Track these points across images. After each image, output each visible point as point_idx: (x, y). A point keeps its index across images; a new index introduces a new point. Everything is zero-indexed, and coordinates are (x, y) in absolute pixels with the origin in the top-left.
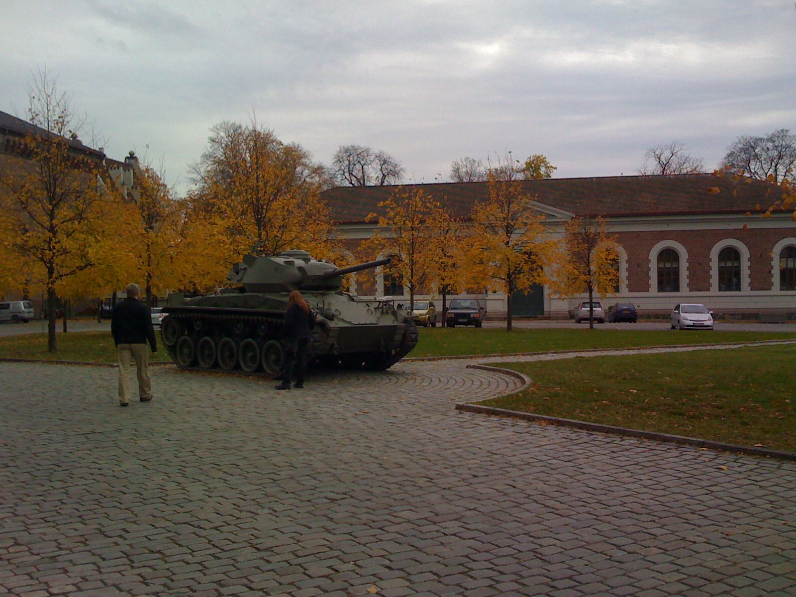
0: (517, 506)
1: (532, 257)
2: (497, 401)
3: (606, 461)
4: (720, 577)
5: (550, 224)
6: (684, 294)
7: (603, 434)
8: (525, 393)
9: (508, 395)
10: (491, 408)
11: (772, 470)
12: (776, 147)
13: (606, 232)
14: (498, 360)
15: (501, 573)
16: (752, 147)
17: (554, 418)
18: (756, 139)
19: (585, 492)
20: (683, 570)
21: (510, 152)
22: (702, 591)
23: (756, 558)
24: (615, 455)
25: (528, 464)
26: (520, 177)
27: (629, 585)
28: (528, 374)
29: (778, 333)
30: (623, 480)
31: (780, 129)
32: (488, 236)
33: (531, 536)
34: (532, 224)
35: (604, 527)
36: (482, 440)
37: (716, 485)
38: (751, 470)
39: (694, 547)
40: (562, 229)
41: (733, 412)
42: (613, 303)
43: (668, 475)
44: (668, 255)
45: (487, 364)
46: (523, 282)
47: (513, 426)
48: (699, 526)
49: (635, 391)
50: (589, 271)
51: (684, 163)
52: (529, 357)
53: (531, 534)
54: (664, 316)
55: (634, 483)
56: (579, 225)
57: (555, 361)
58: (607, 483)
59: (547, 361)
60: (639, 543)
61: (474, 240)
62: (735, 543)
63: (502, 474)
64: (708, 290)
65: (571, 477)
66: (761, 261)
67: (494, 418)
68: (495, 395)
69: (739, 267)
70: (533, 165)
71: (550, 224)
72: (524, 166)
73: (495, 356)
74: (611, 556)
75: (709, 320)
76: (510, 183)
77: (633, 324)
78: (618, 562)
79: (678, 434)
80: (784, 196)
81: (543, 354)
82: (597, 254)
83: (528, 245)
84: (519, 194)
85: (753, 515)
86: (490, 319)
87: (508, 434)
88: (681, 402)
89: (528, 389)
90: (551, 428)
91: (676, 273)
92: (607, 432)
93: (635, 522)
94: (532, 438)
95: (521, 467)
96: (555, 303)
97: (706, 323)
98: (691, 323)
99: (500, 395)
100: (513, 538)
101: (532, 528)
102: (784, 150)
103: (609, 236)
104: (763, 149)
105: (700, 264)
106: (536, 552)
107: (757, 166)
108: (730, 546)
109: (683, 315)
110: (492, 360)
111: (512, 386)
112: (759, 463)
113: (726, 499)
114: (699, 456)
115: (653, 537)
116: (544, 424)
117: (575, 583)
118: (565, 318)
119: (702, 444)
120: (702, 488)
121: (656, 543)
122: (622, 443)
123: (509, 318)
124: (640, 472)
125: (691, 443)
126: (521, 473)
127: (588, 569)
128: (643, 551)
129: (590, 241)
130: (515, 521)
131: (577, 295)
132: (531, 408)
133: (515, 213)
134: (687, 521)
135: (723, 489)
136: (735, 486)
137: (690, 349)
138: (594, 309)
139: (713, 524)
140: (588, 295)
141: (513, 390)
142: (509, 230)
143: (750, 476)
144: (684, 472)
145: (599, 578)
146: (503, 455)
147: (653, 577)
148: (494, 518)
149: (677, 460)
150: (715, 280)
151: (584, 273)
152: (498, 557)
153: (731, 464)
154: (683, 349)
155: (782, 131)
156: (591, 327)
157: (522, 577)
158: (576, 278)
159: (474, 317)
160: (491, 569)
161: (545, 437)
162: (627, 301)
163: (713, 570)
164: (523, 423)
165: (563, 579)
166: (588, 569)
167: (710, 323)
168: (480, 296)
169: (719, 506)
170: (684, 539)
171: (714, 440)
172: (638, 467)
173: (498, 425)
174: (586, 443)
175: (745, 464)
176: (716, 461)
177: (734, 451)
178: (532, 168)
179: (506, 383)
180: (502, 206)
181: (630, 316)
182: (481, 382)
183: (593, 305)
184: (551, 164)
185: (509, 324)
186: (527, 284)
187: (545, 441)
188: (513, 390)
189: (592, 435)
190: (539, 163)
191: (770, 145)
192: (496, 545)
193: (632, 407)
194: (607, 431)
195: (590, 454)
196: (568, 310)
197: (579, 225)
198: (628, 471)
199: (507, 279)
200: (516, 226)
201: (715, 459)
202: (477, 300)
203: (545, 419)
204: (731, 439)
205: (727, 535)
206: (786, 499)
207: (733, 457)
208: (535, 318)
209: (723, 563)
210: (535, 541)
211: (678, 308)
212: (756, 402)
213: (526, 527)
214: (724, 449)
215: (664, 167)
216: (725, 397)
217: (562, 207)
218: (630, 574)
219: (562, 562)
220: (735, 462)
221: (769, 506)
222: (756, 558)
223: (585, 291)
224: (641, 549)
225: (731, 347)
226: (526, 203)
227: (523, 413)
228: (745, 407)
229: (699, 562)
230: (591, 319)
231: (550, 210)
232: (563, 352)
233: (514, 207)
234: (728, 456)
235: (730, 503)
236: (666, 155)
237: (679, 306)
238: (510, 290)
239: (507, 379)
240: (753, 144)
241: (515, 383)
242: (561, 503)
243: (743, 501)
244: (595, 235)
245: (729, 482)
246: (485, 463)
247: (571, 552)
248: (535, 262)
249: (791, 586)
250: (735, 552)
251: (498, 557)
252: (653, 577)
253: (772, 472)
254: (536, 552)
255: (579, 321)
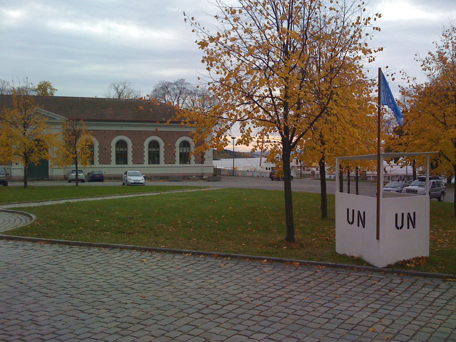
0: (22, 295)
1: (40, 143)
2: (13, 231)
3: (79, 263)
4: (138, 321)
5: (51, 123)
6: (97, 166)
7: (78, 247)
8: (32, 225)
9: (21, 228)
10: (9, 236)
11: (169, 259)
12: (179, 88)
13: (86, 129)
14: (17, 206)
15: (10, 335)
16: (166, 87)
17: (49, 239)
18: (168, 83)
19: (65, 282)
20: (118, 320)
21: (27, 78)
22: (128, 330)
23: (158, 308)
24: (84, 259)
25: (31, 268)
26: (35, 94)
27: (88, 332)
28: (34, 214)
29: (177, 187)
30: (88, 273)
31: (180, 79)
32: (12, 129)
33: (30, 311)
34: (40, 123)
35: (75, 301)
36: (2, 256)
37: (140, 270)
38: (159, 260)
39: (126, 306)
40: (60, 127)
41: (151, 230)
42: (90, 171)
43: (114, 267)
44: (122, 144)
45: (9, 209)
46: (34, 158)
47: (23, 246)
48: (129, 294)
49: (98, 221)
50: (76, 152)
51: (131, 93)
52: (37, 203)
53: (31, 310)
54: (118, 178)
55: (94, 273)
56: (70, 125)
57: (52, 206)
58: (78, 275)
59: (47, 206)
60: (95, 308)
61: (3, 131)
62: (147, 301)
63: (14, 276)
64: (143, 163)
65: (57, 274)
66: (169, 149)
67: (11, 242)
68: (12, 228)
69: (159, 151)
70: (43, 87)
71: (52, 123)
72: (37, 87)
73: (14, 204)
74: (78, 317)
75: (143, 180)
76: (27, 97)
77: (101, 183)
78: (82, 320)
79: (121, 243)
80: (177, 113)
81: (45, 201)
82: (81, 141)
83: (38, 135)
84: (32, 104)
85: (158, 285)
86: (15, 181)
87: (19, 251)
88: (123, 225)
89: (34, 222)
90: (47, 245)
91: (126, 154)
92: (81, 246)
93: (93, 296)
94: (34, 252)
95: (27, 271)
96: (55, 171)
97: (141, 182)
98: (133, 182)
99: (15, 228)
100: (19, 314)
101: (31, 306)
102: (182, 90)
103: (87, 132)
104: (172, 89)
105: (138, 149)
106: (33, 320)
107: (169, 98)
108: (145, 304)
109: (129, 177)
110: (12, 206)
111: (24, 221)
112: (163, 256)
113: (144, 277)
114: (132, 255)
115: (103, 303)
116: (43, 244)
117: (56, 336)
118: (61, 180)
119: (133, 248)
120: (132, 272)
121: (105, 306)
122: (89, 251)
123: (25, 180)
124: (98, 267)
125: (127, 248)
126: (27, 274)
127: (65, 326)
128: (97, 312)
129: (77, 135)
130: (21, 303)
131: (68, 166)
132: (35, 234)
133: (30, 116)
134: (123, 292)
135: (143, 272)
136: (150, 270)
137: (132, 196)
138: (78, 174)
139: (137, 292)
140: (74, 166)
141: (24, 224)
142: (25, 126)
143: (158, 264)
144: (123, 265)
145: (70, 331)
146: (15, 264)
147: (102, 326)
148: (7, 303)
149: (119, 258)
150: (146, 158)
151: (73, 153)
152: (9, 326)
153: (149, 258)
154: (128, 196)
155: (182, 80)
156: (77, 185)
157: (23, 336)
158: (68, 156)
159: (3, 180)
160: (4, 334)
161: (43, 251)
162: (98, 170)
163: (135, 318)
164: (30, 244)
165: (49, 334)
166: (65, 326)
167: (143, 181)
168: (6, 166)
169: (141, 281)
170: (120, 302)
171: (140, 245)
172: (97, 264)
173: (13, 246)
174: (68, 253)
175: (156, 257)
176: (140, 257)
177: (150, 250)
178: (42, 89)
179: (20, 220)
180: (21, 111)
181: (100, 178)
182: (4, 220)
183: (78, 172)
184: (54, 88)
185: (26, 184)
186: (37, 159)
187: (42, 254)
188: (24, 224)
189: (72, 248)
190: (418, 104)
191: (175, 87)
192: (8, 319)
193: (96, 230)
194: (81, 245)
195: (70, 259)
196: (63, 175)
197: (70, 125)
198: (91, 267)
199: (24, 156)
200: (30, 124)
201: (140, 256)
202: (5, 169)
203: (43, 241)
204: (149, 244)
205: (144, 297)
206: (176, 274)
207: (150, 254)
208: (43, 180)
209: (141, 313)
210: (33, 314)
211: (126, 173)
212: (163, 223)
213: (27, 307)
214: (145, 250)
215: (120, 94)
216: (147, 222)
217: (60, 113)
218: (88, 326)
219: (49, 324)
220: (150, 256)
221: (167, 279)
222: (158, 308)
223: (72, 164)
224: (96, 311)
225: (154, 194)
226: (37, 110)
227: (30, 238)
228: (157, 226)
229: (128, 314)
230: (77, 180)
231: (52, 114)
232: (59, 200)
233: (29, 112)
234: (147, 254)
235: (147, 280)
236: (121, 87)
237: (126, 172)
238: (26, 162)
239: (21, 218)
240: (167, 86)
241: (26, 220)
242: (50, 290)
243: (153, 277)
244: (79, 131)
245: (147, 268)
246: (3, 270)
247: (55, 318)
248: (42, 146)
249: (175, 321)
250: (147, 306)
251: (9, 326)
252: (102, 326)
253: (169, 261)
254: (33, 320)
255: (70, 181)
